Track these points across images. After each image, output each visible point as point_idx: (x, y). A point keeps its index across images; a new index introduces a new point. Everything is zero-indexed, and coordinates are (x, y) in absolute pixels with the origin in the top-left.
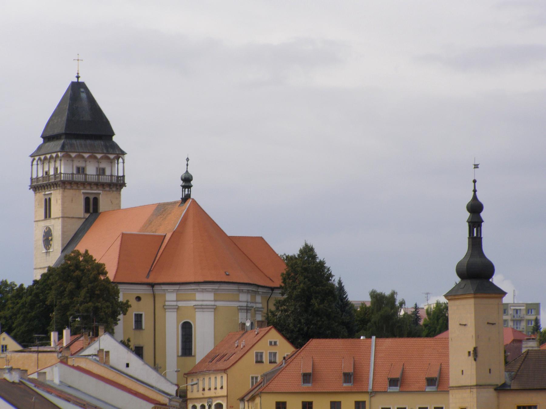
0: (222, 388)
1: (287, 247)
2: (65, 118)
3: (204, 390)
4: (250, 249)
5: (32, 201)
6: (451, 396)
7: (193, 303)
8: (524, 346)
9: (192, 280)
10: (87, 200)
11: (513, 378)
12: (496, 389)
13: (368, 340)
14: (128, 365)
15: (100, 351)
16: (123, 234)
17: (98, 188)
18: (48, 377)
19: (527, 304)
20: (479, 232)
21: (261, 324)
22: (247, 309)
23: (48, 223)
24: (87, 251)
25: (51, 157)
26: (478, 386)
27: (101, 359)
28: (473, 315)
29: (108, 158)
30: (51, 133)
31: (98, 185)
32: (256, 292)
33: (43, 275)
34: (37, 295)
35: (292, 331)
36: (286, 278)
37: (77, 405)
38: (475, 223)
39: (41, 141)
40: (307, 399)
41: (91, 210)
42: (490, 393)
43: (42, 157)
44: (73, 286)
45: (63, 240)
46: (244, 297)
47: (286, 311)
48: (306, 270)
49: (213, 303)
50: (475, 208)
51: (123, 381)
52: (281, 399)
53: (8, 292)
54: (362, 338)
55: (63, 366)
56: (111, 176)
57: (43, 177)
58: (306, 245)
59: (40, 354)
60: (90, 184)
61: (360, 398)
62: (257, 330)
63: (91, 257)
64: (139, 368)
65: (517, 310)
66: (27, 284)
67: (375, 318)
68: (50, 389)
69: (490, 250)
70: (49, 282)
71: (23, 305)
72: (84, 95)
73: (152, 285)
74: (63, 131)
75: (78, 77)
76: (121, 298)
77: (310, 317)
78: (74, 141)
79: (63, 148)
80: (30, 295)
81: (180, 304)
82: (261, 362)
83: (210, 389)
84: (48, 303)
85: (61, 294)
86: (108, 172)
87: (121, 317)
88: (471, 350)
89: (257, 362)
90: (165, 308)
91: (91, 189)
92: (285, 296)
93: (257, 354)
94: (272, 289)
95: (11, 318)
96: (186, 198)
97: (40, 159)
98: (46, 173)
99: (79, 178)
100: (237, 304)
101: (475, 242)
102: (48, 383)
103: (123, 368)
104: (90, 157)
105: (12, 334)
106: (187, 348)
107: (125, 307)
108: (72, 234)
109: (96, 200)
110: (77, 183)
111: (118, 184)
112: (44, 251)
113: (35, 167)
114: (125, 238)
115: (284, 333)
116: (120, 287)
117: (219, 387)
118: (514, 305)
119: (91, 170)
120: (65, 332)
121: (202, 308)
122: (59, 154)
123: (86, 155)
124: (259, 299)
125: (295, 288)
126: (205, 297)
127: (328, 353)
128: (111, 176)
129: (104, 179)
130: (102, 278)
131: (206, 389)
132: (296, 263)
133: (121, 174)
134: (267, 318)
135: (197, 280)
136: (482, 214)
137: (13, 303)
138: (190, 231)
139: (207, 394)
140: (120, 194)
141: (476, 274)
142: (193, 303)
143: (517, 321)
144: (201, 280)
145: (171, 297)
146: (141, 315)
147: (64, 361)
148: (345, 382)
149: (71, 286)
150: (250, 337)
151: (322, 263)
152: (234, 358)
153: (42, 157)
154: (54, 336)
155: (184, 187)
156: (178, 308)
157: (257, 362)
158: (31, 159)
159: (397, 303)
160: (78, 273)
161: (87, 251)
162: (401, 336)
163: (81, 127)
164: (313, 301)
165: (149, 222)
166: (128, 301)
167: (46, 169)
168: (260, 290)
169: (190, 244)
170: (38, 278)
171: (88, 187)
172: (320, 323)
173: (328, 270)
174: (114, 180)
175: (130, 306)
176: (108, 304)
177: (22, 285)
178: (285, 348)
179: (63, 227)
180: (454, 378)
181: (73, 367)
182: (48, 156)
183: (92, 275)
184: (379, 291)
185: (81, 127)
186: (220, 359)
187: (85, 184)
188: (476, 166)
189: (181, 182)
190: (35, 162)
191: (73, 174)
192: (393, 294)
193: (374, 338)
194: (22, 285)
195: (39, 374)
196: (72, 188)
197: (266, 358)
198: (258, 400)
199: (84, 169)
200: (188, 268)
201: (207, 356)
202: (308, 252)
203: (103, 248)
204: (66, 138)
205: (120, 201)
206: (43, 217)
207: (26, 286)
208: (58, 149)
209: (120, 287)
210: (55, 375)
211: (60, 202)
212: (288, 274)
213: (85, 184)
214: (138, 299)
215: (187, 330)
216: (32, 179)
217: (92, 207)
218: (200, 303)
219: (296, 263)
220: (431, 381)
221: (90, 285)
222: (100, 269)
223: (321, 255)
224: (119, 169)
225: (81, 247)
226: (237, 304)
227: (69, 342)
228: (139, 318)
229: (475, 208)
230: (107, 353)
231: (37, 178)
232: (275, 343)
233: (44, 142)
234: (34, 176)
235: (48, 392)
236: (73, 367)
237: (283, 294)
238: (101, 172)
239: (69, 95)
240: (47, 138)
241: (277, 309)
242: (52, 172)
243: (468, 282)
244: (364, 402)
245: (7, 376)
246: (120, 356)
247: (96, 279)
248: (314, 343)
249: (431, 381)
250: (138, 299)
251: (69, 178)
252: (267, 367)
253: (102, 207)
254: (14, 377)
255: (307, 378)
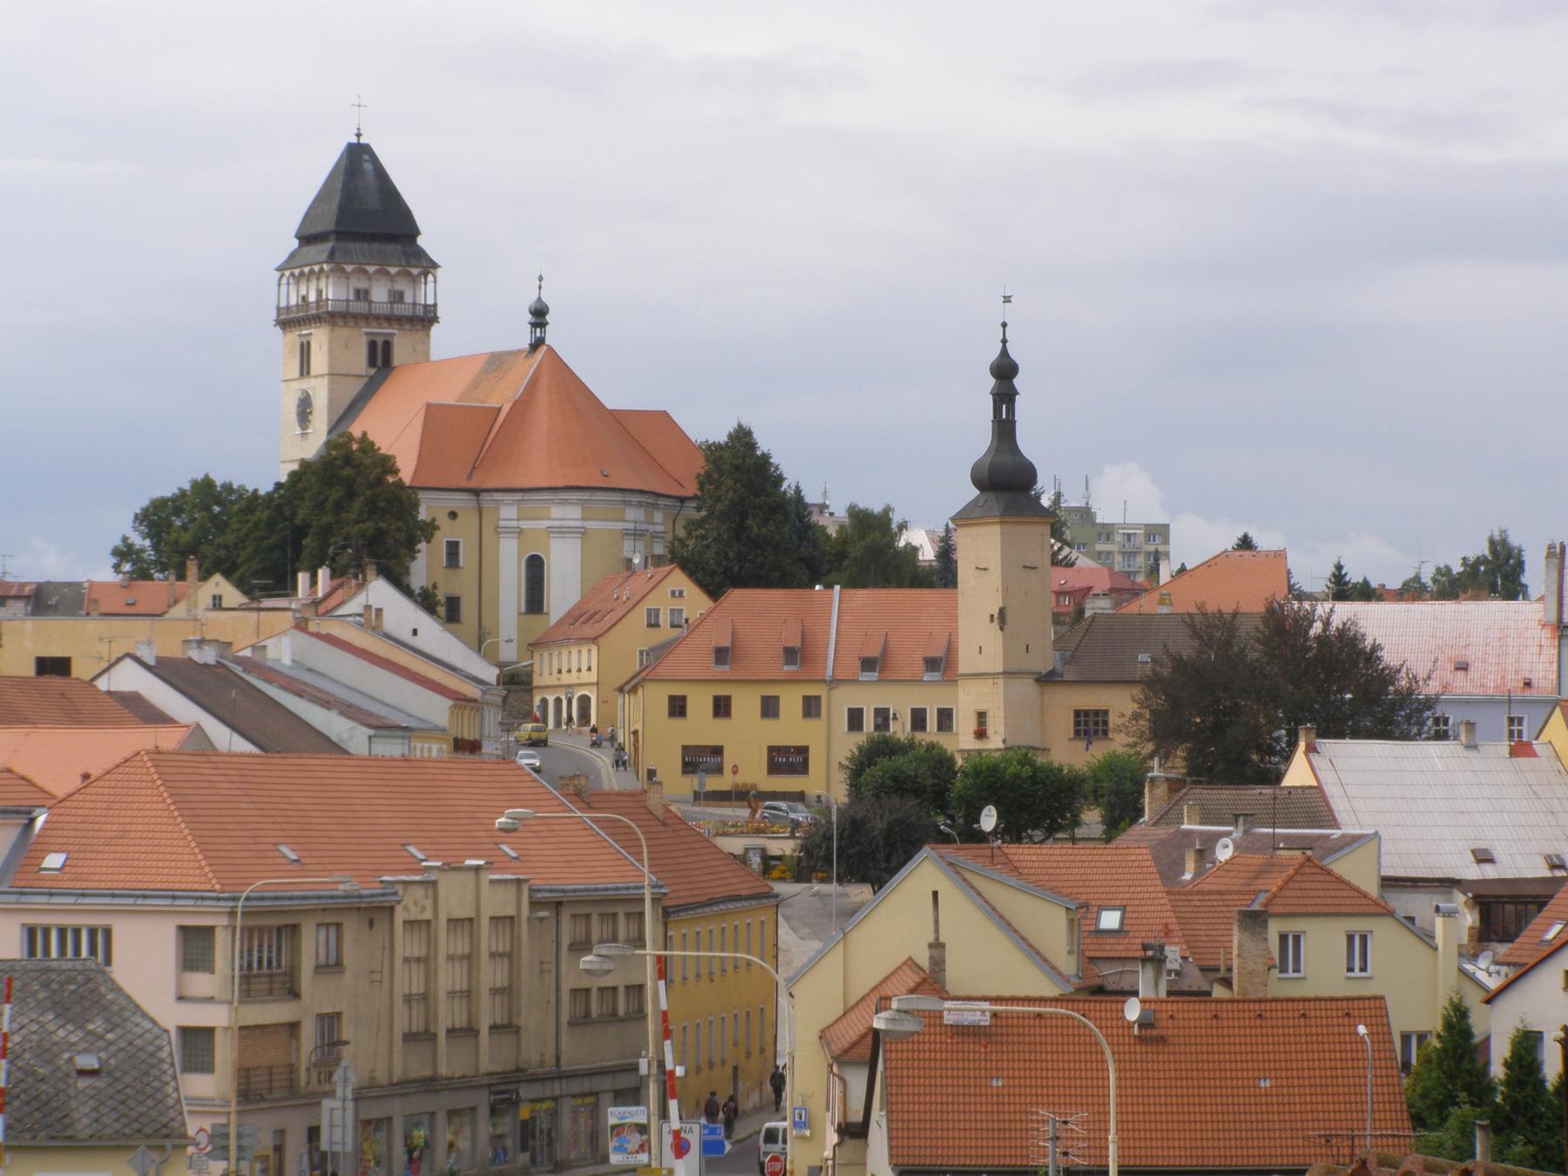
0: (589, 669)
1: (707, 425)
2: (335, 205)
3: (560, 672)
4: (645, 432)
5: (282, 345)
6: (960, 691)
7: (544, 524)
8: (1088, 606)
9: (546, 484)
10: (372, 346)
11: (1067, 662)
12: (1037, 681)
13: (828, 592)
14: (415, 632)
15: (368, 607)
16: (429, 406)
17: (390, 326)
18: (271, 654)
19: (1147, 525)
20: (1011, 411)
21: (658, 561)
22: (636, 534)
23: (306, 384)
24: (365, 434)
25: (312, 272)
26: (1007, 674)
27: (368, 620)
28: (999, 552)
29: (410, 274)
30: (312, 231)
31: (391, 319)
32: (655, 506)
33: (292, 474)
34: (279, 508)
35: (713, 573)
36: (704, 481)
37: (314, 702)
38: (1005, 395)
39: (295, 243)
40: (722, 691)
41: (379, 362)
42: (1028, 687)
43: (297, 272)
44: (341, 494)
45: (330, 414)
46: (634, 515)
47: (703, 537)
48: (737, 468)
49: (578, 524)
50: (1005, 370)
51: (405, 659)
52: (678, 690)
53: (234, 503)
54: (817, 587)
55: (302, 636)
56: (414, 304)
57: (297, 305)
58: (740, 426)
59: (262, 614)
60: (377, 318)
61: (812, 691)
62: (651, 570)
63: (372, 444)
64: (433, 635)
65: (1129, 536)
66: (265, 488)
67: (855, 551)
68: (271, 674)
69: (1028, 442)
70: (300, 486)
71: (256, 525)
72: (368, 167)
73: (477, 492)
74: (332, 227)
75: (359, 135)
76: (423, 515)
77: (744, 549)
78: (351, 246)
79: (331, 257)
80: (268, 508)
81: (524, 525)
82: (658, 626)
83: (569, 671)
84: (298, 521)
85: (320, 507)
86: (408, 299)
87: (422, 546)
88: (996, 613)
89: (650, 625)
90: (497, 531)
91: (380, 326)
92: (703, 513)
93: (649, 611)
94: (682, 500)
95: (236, 546)
96: (537, 344)
97: (292, 275)
98: (304, 298)
99: (360, 307)
100: (621, 526)
101: (1004, 429)
102: (270, 664)
103: (406, 636)
104: (378, 271)
105: (236, 575)
106: (535, 600)
107: (429, 529)
108: (346, 402)
109: (387, 346)
110: (355, 317)
111: (426, 319)
112: (299, 431)
113: (284, 288)
114: (433, 413)
115: (700, 575)
116: (421, 495)
117: (584, 668)
118: (1125, 525)
119: (380, 294)
120: (320, 572)
121: (562, 532)
122: (325, 267)
123: (371, 269)
124: (658, 517)
125: (718, 499)
126: (567, 513)
127: (762, 613)
128: (414, 304)
129: (402, 310)
130: (391, 479)
131: (564, 670)
132: (721, 457)
133: (430, 301)
134: (672, 551)
135: (553, 485)
136: (1016, 381)
137: (240, 521)
138: (543, 399)
139: (566, 679)
140: (428, 335)
141: (1006, 482)
142: (544, 524)
143: (1129, 555)
144: (560, 484)
145: (508, 513)
146: (457, 543)
147: (301, 626)
148: (787, 663)
149: (336, 493)
150: (638, 584)
151: (765, 458)
152: (609, 620)
153: (297, 272)
154: (302, 578)
155: (534, 325)
156: (520, 532)
157: (650, 625)
158: (278, 274)
159: (894, 526)
160: (348, 471)
161: (365, 434)
162: (900, 584)
163: (363, 219)
164: (750, 522)
165: (475, 384)
166: (434, 520)
167: (303, 292)
168: (662, 502)
169: (542, 419)
170: (283, 479)
171: (374, 324)
172: (761, 559)
173: (777, 468)
174: (420, 312)
175: (438, 528)
176: (400, 524)
177: (256, 491)
178: (695, 602)
179: (331, 391)
180: (966, 661)
181: (317, 636)
182: (306, 270)
183: (373, 476)
184: (862, 505)
185: (363, 219)
186: (589, 620)
187: (369, 318)
188: (1007, 299)
189: (529, 317)
190: (284, 281)
191: (348, 301)
192: (887, 510)
193: (837, 588)
194: (256, 491)
195: (253, 647)
196: (346, 325)
197: (664, 619)
198: (640, 691)
199: (367, 292)
200: (537, 466)
201: (568, 614)
202: (742, 438)
203: (394, 431)
204: (337, 239)
205: (428, 348)
206: (297, 374)
207: (262, 492)
208: (324, 257)
209: (421, 495)
210: (283, 650)
211: (325, 348)
212: (708, 475)
213: (369, 318)
214: (453, 515)
215: (535, 569)
216: (278, 309)
217: (381, 358)
218: (558, 523)
219: (721, 457)
220: (932, 664)
221: (369, 492)
222: (387, 464)
223: (764, 444)
224: (427, 293)
225: (356, 430)
226: (621, 526)
227: (328, 590)
228: (453, 548)
229: (1005, 370)
230: (379, 611)
231: (288, 308)
232: (681, 593)
233: (301, 246)
234: (283, 304)
235: (267, 680)
236: (317, 636)
237: (699, 509)
238: (398, 297)
239: (343, 167)
240: (307, 238)
241: (689, 534)
242: (312, 298)
243: (992, 495)
244: (818, 698)
245: (195, 654)
246: (400, 613)
247: (380, 481)
248: (736, 596)
249: (932, 664)
250: (453, 515)
251: (342, 307)
252: (665, 633)
253: (398, 357)
254: (208, 656)
255: (721, 655)
